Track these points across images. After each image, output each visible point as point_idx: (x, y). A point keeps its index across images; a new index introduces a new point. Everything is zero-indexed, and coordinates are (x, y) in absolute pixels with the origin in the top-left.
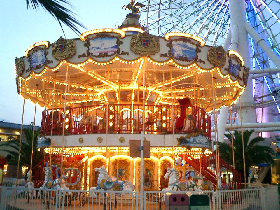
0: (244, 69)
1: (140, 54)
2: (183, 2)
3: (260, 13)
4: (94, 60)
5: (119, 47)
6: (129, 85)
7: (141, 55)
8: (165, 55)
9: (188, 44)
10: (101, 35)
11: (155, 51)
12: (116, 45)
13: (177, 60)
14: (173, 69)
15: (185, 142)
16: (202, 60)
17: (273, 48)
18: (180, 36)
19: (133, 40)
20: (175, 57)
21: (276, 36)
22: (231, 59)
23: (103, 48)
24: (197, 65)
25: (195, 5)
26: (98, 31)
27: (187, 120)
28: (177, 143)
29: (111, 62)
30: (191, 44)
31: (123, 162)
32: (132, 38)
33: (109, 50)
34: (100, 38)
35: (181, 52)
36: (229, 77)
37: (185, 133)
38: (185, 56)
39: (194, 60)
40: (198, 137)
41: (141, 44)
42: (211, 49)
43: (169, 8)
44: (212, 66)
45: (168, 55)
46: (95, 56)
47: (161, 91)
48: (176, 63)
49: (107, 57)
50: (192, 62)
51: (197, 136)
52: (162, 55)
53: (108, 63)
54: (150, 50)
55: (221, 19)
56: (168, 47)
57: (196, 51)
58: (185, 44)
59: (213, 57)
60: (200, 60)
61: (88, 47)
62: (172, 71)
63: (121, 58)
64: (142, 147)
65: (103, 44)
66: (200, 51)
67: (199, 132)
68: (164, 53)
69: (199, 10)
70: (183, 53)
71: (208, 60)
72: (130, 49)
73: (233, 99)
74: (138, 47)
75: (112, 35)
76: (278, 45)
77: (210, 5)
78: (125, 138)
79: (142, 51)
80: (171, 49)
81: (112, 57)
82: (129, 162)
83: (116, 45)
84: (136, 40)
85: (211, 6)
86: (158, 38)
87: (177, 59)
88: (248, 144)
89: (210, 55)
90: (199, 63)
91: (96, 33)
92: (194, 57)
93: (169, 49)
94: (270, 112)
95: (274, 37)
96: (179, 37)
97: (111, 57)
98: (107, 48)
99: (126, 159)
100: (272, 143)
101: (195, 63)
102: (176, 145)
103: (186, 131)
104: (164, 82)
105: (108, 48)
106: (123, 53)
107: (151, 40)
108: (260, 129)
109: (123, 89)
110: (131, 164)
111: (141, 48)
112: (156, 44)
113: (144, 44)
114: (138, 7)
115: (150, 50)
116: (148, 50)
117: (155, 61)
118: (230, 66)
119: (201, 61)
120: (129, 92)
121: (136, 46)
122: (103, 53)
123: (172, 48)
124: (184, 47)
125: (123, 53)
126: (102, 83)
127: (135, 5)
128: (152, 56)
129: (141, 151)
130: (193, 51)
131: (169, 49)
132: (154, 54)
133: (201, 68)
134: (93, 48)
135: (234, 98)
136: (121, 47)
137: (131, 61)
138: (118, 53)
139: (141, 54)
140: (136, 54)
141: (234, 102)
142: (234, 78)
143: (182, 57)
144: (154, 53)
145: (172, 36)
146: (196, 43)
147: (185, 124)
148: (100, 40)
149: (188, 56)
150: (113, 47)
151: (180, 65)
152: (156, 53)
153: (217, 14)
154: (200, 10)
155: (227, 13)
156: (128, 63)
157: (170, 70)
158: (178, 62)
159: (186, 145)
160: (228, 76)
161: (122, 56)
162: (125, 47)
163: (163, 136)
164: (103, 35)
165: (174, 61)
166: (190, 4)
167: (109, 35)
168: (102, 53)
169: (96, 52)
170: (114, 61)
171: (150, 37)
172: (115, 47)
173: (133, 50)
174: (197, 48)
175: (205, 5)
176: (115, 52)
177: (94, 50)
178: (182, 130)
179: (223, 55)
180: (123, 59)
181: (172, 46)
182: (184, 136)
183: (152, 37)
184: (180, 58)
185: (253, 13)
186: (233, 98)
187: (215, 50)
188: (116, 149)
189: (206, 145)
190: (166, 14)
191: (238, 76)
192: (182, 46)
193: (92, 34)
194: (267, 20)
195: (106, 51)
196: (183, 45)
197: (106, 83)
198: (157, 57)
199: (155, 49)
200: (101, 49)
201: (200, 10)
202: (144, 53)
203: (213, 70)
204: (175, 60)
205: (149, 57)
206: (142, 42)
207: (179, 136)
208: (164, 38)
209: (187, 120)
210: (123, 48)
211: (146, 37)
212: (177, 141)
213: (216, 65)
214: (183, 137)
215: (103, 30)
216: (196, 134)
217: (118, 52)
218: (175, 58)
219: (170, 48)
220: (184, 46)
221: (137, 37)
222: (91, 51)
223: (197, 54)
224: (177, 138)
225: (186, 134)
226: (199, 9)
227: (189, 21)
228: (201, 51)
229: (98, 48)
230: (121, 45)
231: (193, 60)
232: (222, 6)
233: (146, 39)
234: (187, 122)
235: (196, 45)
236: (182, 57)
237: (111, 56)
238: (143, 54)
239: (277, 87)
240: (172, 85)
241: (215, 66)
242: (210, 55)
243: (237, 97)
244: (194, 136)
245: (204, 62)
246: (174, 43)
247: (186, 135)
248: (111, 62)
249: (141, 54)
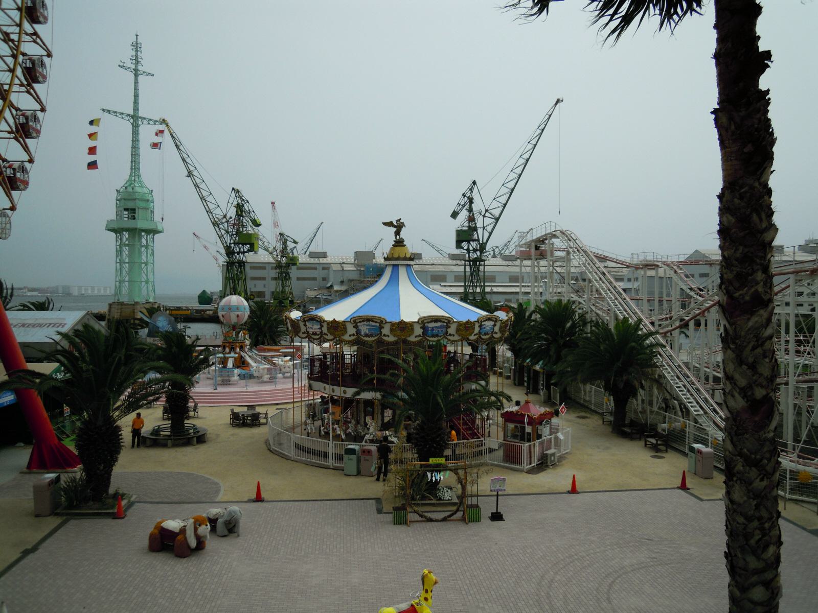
9: (371, 323)
106: (450, 335)
146: (378, 321)
220: (369, 325)
227: (39, 142)
245: (454, 335)
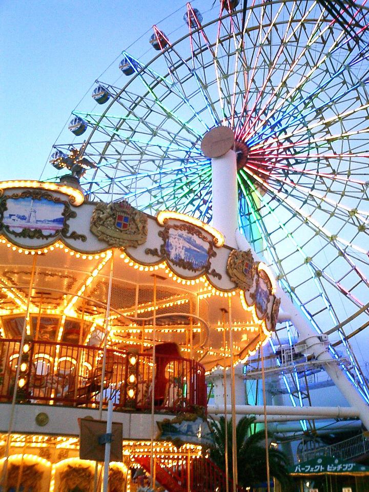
0: (274, 301)
1: (108, 242)
2: (133, 186)
3: (261, 220)
5: (68, 222)
6: (56, 308)
8: (154, 252)
11: (137, 241)
12: (62, 217)
13: (174, 265)
15: (171, 432)
16: (217, 271)
17: (280, 278)
18: (184, 221)
19: (98, 213)
20: (171, 258)
22: (260, 279)
23: (32, 219)
24: (208, 279)
25: (154, 193)
26: (28, 185)
27: (172, 386)
30: (201, 240)
32: (96, 210)
34: (30, 199)
35: (183, 251)
37: (171, 411)
38: (189, 259)
39: (204, 269)
40: (195, 423)
41: (112, 223)
44: (232, 286)
45: (160, 253)
46: (13, 233)
47: (115, 325)
49: (38, 238)
50: (200, 272)
51: (194, 420)
52: (149, 252)
56: (161, 239)
57: (208, 253)
59: (236, 269)
60: (214, 271)
63: (67, 245)
66: (214, 255)
67: (199, 413)
69: (159, 203)
70: (186, 253)
71: (227, 273)
72: (89, 228)
73: (238, 355)
75: (55, 196)
76: (285, 276)
78: (49, 415)
79: (114, 238)
80: (165, 242)
81: (50, 240)
82: (41, 470)
83: (62, 217)
85: (182, 197)
86: (145, 218)
87: (175, 263)
88: (244, 443)
90: (211, 277)
92: (204, 265)
93: (162, 243)
94: (267, 389)
100: (272, 444)
101: (204, 276)
104: (137, 306)
106: (74, 236)
110: (45, 475)
112: (140, 229)
113: (119, 224)
114: (84, 166)
116: (125, 236)
118: (257, 291)
120: (55, 321)
121: (103, 225)
123: (167, 240)
125: (74, 236)
128: (130, 251)
129: (106, 444)
130: (203, 252)
131: (162, 243)
132: (135, 247)
135: (240, 355)
136: (70, 222)
137: (87, 253)
138: (63, 233)
139: (111, 242)
140: (101, 240)
141: (240, 361)
143: (184, 260)
144: (135, 245)
145: (170, 219)
146: (210, 238)
148: (28, 203)
149: (193, 261)
150: (54, 221)
151: (179, 275)
153: (191, 212)
154: (161, 203)
156: (81, 256)
157: (153, 284)
158: (177, 269)
159: (174, 438)
160: (252, 309)
161: (71, 242)
162: (80, 224)
163: (127, 415)
165: (169, 266)
167: (50, 196)
168: (29, 229)
170: (52, 248)
171: (132, 213)
172: (58, 222)
173: (95, 231)
174: (211, 249)
176: (57, 231)
177: (14, 220)
178: (162, 406)
180: (72, 248)
181: (168, 237)
182: (171, 418)
183: (136, 214)
184: (181, 263)
186: (238, 353)
187: (241, 257)
188: (18, 440)
189: (208, 439)
191: (266, 310)
195: (39, 225)
196: (187, 238)
198: (139, 253)
201: (161, 203)
203: (234, 293)
204: (171, 264)
205: (125, 251)
206: (115, 219)
207: (161, 418)
208: (155, 219)
209: (172, 386)
210: (75, 225)
211: (124, 212)
212: (157, 429)
213: (239, 285)
214: (169, 420)
216: (193, 416)
217: (64, 231)
218: (172, 261)
219: (164, 240)
220: (189, 241)
221: (107, 209)
224: (158, 423)
225: (174, 415)
226: (161, 200)
230: (71, 219)
231: (201, 270)
233: (123, 214)
234: (171, 389)
235: (210, 243)
236: (184, 260)
237: (47, 237)
239: (282, 346)
240: (155, 313)
241: (237, 286)
243: (250, 352)
244: (188, 420)
246: (171, 231)
248: (39, 252)
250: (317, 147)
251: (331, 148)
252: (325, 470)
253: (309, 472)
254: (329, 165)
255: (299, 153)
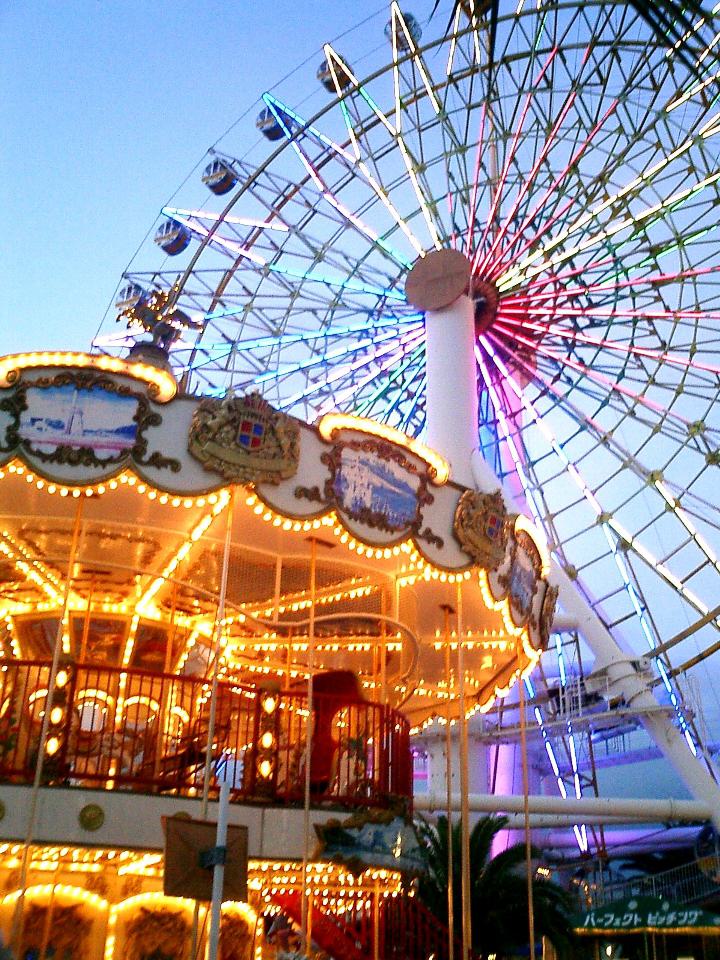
2: (274, 357)
4: (31, 468)
5: (145, 434)
6: (120, 600)
7: (227, 479)
8: (311, 494)
9: (392, 466)
10: (79, 376)
11: (278, 472)
12: (134, 423)
14: (325, 557)
18: (369, 434)
21: (556, 515)
23: (76, 428)
24: (417, 547)
25: (312, 373)
26: (69, 361)
27: (346, 754)
28: (314, 845)
29: (89, 492)
30: (404, 470)
31: (64, 919)
33: (103, 440)
34: (71, 388)
36: (506, 612)
37: (342, 804)
38: (381, 508)
39: (410, 527)
41: (231, 436)
42: (467, 499)
43: (224, 366)
44: (464, 560)
45: (323, 496)
46: (39, 454)
48: (346, 528)
49: (87, 464)
52: (303, 493)
53: (77, 492)
54: (265, 464)
55: (490, 407)
57: (418, 496)
58: (384, 467)
60: (428, 531)
61: (16, 416)
62: (317, 561)
63: (144, 479)
64: (224, 850)
65: (81, 413)
66: (430, 499)
68: (309, 486)
69: (321, 393)
74: (221, 445)
75: (121, 382)
77: (363, 382)
79: (234, 465)
81: (110, 468)
82: (88, 916)
84: (217, 420)
87: (352, 515)
89: (462, 521)
90: (422, 543)
91: (57, 363)
95: (551, 517)
96: (367, 438)
97: (104, 467)
98: (95, 429)
99: (180, 913)
101: (410, 541)
102: (311, 855)
103: (337, 798)
105: (100, 430)
106: (157, 461)
107: (272, 428)
108: (573, 818)
109: (103, 614)
110: (95, 927)
111: (229, 453)
112: (286, 448)
113: (244, 439)
114: (176, 325)
115: (265, 464)
116: (256, 462)
117: (277, 511)
119: (431, 538)
120: (117, 626)
121: (213, 440)
122: (77, 448)
124: (378, 475)
125: (157, 461)
126: (21, 578)
127: (169, 316)
128: (266, 491)
130: (408, 495)
131: (329, 475)
132: (274, 484)
133: (428, 560)
134: (37, 423)
135: (479, 696)
136: (151, 434)
137: (183, 494)
138: (135, 456)
139: (229, 473)
140: (209, 470)
141: (478, 707)
142: (519, 618)
144: (275, 479)
147: (338, 773)
148: (68, 397)
150: (119, 431)
151: (360, 540)
152: (282, 479)
153: (383, 415)
154: (327, 393)
155: (415, 417)
158: (355, 525)
159: (348, 857)
160: (503, 607)
161: (151, 472)
163: (257, 811)
164: (86, 379)
165: (340, 521)
166: (296, 367)
167: (110, 382)
168: (69, 447)
169: (44, 439)
170: (113, 484)
174: (423, 488)
175: (346, 380)
176: (124, 452)
177: (40, 429)
178: (326, 793)
179: (502, 525)
180: (152, 485)
181: (340, 465)
182: (343, 817)
183: (277, 419)
184: (363, 515)
185: (495, 433)
190: (210, 384)
192: (372, 469)
193: (40, 368)
194: (535, 463)
195: (89, 440)
197: (33, 576)
198: (283, 495)
199: (282, 464)
200: (69, 432)
201: (327, 393)
202: (240, 474)
203: (467, 575)
204: (345, 517)
205: (255, 491)
206: (236, 428)
207: (323, 817)
208: (315, 429)
209: (346, 754)
210: (158, 440)
211: (253, 415)
212: (316, 839)
213: (478, 559)
214: (338, 822)
215: (90, 359)
217: (138, 451)
218: (347, 511)
219: (333, 471)
220: (381, 472)
222: (25, 432)
223: (423, 511)
224: (317, 827)
226: (326, 389)
228: (436, 500)
229: (58, 425)
232: (399, 391)
234: (344, 762)
235: (421, 476)
237: (104, 463)
238: (235, 474)
241: (474, 561)
242: (462, 521)
243: (498, 691)
244: (376, 821)
245: (440, 543)
246: (346, 453)
247: (349, 815)
248: (89, 492)
249: (226, 475)
250: (634, 295)
251: (659, 299)
252: (644, 924)
253: (611, 926)
254: (654, 332)
255: (598, 305)
